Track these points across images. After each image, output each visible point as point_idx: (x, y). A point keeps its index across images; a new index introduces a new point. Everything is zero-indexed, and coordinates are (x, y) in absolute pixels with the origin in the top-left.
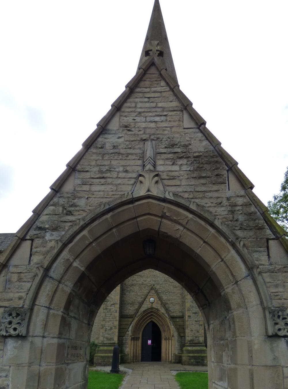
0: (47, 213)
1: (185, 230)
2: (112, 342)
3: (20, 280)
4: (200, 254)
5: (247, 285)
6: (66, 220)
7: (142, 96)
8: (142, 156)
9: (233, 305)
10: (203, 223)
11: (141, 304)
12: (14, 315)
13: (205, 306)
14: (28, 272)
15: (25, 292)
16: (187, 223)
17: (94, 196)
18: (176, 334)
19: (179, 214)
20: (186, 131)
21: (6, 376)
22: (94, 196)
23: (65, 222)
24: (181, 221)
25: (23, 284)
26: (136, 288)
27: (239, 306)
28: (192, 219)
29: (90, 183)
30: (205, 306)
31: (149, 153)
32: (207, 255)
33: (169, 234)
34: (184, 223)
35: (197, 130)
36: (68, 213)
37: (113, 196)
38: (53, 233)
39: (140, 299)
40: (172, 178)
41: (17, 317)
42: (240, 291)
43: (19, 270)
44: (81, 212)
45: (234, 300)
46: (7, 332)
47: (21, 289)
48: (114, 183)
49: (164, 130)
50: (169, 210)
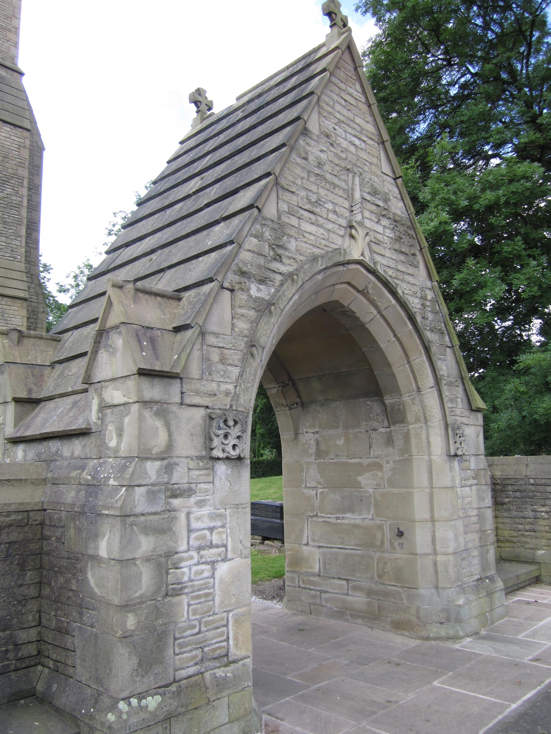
0: (250, 248)
1: (378, 316)
3: (223, 360)
4: (383, 349)
5: (431, 400)
6: (275, 269)
7: (338, 92)
9: (410, 417)
10: (403, 314)
12: (231, 423)
13: (295, 405)
14: (233, 348)
15: (232, 383)
16: (386, 308)
17: (305, 240)
19: (381, 295)
20: (383, 175)
21: (223, 526)
22: (305, 240)
23: (274, 271)
24: (379, 304)
25: (230, 368)
27: (417, 420)
28: (393, 305)
29: (299, 215)
30: (295, 405)
32: (393, 354)
33: (358, 315)
34: (382, 308)
35: (393, 181)
36: (278, 257)
37: (324, 248)
38: (261, 287)
40: (378, 242)
41: (234, 426)
42: (422, 402)
43: (220, 342)
44: (292, 260)
45: (413, 411)
46: (223, 451)
47: (228, 377)
48: (325, 226)
49: (365, 164)
50: (375, 287)
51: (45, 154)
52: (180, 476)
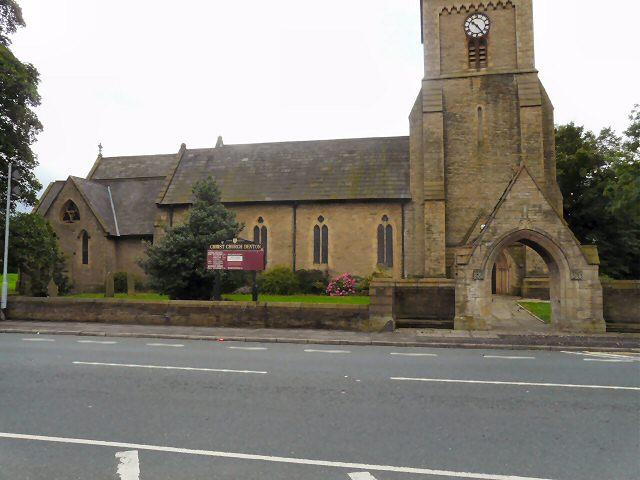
2: (439, 273)
8: (522, 212)
11: (470, 231)
18: (514, 264)
26: (463, 213)
31: (525, 210)
39: (468, 226)
51: (555, 113)
52: (468, 282)
